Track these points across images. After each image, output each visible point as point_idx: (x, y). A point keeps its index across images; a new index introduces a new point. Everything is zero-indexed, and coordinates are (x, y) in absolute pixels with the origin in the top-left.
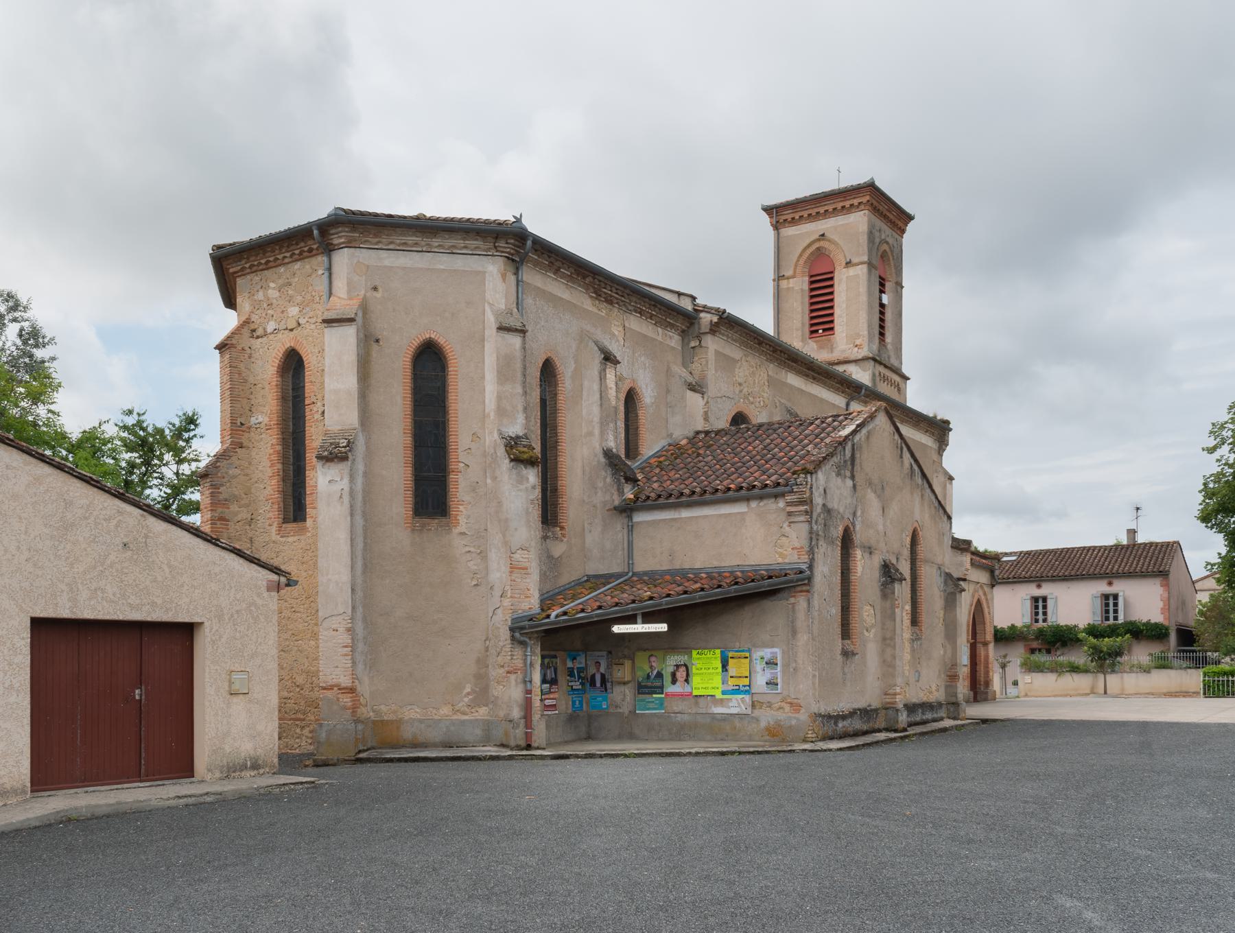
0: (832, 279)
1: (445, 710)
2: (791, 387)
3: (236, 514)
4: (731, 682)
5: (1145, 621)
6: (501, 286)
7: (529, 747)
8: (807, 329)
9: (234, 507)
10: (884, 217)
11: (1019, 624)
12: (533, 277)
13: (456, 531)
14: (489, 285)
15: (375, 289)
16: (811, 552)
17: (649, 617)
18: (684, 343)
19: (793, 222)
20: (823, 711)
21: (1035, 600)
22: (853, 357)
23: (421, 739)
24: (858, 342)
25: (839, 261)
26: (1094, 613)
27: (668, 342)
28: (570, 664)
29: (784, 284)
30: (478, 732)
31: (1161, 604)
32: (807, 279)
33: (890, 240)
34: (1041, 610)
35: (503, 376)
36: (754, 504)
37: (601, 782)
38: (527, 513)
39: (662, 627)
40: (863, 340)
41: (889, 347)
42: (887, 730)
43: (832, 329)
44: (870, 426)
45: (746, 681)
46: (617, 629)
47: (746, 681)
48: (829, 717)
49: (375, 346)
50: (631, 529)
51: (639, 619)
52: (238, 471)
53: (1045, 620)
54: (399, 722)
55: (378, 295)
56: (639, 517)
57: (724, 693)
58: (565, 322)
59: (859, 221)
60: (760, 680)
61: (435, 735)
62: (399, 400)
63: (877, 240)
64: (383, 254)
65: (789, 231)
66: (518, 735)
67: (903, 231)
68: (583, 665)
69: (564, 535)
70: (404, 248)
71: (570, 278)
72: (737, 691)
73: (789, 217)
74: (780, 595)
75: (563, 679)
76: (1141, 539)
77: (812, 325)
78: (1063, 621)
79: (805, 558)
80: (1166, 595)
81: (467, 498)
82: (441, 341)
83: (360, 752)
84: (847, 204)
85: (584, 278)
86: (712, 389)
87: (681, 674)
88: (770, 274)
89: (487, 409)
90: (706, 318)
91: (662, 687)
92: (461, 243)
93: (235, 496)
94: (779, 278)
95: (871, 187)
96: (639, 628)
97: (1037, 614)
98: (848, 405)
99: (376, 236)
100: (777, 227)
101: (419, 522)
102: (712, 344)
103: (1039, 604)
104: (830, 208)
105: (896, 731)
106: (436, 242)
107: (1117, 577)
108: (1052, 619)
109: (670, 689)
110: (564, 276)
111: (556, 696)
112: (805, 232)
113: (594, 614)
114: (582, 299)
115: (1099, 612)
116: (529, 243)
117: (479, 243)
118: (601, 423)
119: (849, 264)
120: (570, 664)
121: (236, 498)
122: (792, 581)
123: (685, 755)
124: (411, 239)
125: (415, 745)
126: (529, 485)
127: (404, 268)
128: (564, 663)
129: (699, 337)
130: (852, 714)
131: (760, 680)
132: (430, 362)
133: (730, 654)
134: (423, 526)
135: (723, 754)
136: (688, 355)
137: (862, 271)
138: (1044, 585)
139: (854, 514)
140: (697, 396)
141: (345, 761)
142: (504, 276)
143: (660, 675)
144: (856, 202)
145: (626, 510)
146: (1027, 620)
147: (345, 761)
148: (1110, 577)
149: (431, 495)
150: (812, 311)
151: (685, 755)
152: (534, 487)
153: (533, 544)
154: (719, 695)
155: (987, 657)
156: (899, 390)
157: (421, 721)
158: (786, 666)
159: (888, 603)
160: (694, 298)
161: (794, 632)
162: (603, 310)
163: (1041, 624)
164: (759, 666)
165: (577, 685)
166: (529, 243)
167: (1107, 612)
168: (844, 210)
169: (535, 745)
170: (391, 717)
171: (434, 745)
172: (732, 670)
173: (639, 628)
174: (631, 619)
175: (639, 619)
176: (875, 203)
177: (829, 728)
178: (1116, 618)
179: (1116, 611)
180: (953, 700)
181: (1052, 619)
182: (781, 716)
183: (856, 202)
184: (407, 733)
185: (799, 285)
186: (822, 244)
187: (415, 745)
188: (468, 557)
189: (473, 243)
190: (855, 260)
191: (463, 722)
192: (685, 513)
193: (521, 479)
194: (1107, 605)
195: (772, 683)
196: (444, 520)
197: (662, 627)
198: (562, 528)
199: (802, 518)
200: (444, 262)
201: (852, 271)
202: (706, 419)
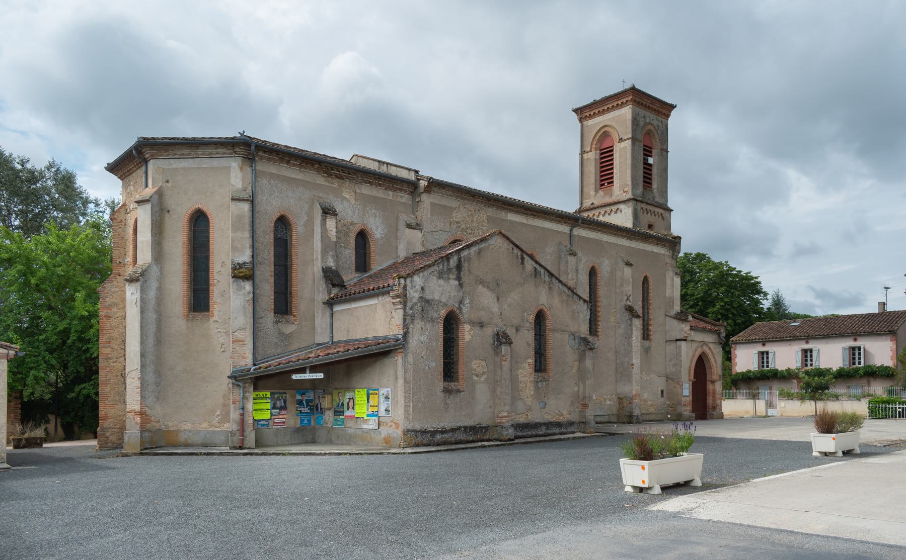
0: (612, 150)
1: (205, 425)
2: (511, 222)
3: (116, 313)
4: (371, 409)
5: (879, 365)
6: (240, 175)
7: (241, 448)
8: (598, 183)
9: (115, 310)
10: (646, 107)
11: (793, 367)
12: (263, 166)
13: (212, 320)
14: (233, 175)
15: (167, 182)
16: (406, 326)
17: (314, 369)
18: (413, 200)
19: (590, 117)
20: (418, 427)
21: (805, 351)
22: (622, 199)
23: (190, 442)
24: (626, 189)
25: (616, 139)
26: (844, 360)
27: (399, 199)
28: (299, 397)
29: (585, 156)
30: (223, 438)
31: (891, 354)
32: (598, 152)
33: (655, 123)
34: (809, 358)
35: (236, 228)
36: (380, 298)
37: (297, 469)
38: (244, 308)
39: (320, 376)
40: (629, 188)
41: (655, 191)
42: (496, 440)
43: (612, 182)
44: (483, 245)
45: (376, 409)
46: (295, 377)
47: (376, 409)
48: (425, 432)
49: (167, 215)
50: (332, 315)
51: (308, 371)
52: (117, 289)
53: (811, 365)
54: (178, 431)
55: (169, 185)
56: (337, 308)
57: (368, 416)
58: (287, 195)
59: (626, 112)
60: (382, 408)
61: (197, 439)
62: (180, 244)
63: (642, 124)
64: (172, 161)
65: (590, 123)
66: (236, 439)
67: (668, 116)
68: (312, 397)
69: (296, 320)
70: (182, 157)
71: (301, 166)
72: (372, 415)
73: (588, 114)
74: (392, 355)
75: (292, 407)
76: (890, 308)
77: (602, 181)
78: (823, 366)
79: (401, 332)
80: (895, 347)
81: (219, 300)
82: (205, 209)
83: (146, 449)
84: (620, 103)
85: (313, 165)
86: (426, 227)
87: (351, 404)
88: (579, 152)
89: (228, 247)
90: (423, 183)
91: (343, 412)
92: (214, 151)
93: (115, 303)
94: (583, 152)
95: (634, 90)
96: (308, 376)
97: (806, 361)
98: (571, 230)
99: (166, 151)
100: (581, 120)
101: (192, 315)
102: (427, 200)
103: (763, 355)
104: (610, 106)
105: (501, 441)
106: (200, 152)
107: (859, 335)
108: (816, 364)
109: (347, 413)
110: (294, 165)
111: (285, 416)
112: (596, 123)
113: (283, 368)
114: (320, 180)
115: (847, 359)
116: (253, 148)
117: (224, 150)
118: (322, 252)
119: (621, 140)
120: (299, 397)
121: (116, 305)
122: (390, 346)
123: (318, 455)
124: (186, 151)
125: (186, 445)
126: (246, 292)
127: (184, 169)
128: (294, 397)
129: (419, 195)
130: (453, 430)
131: (382, 408)
132: (199, 222)
133: (371, 392)
134: (194, 317)
135: (340, 454)
136: (415, 206)
137: (628, 144)
138: (811, 341)
139: (461, 302)
140: (417, 232)
141: (135, 454)
142: (241, 169)
143: (343, 405)
144: (624, 100)
145: (330, 303)
146: (799, 365)
147: (135, 454)
148: (855, 335)
149: (199, 300)
150: (602, 172)
151: (318, 455)
152: (249, 293)
153: (248, 326)
154: (366, 418)
155: (714, 390)
156: (663, 218)
157: (190, 431)
158: (393, 399)
159: (498, 359)
160: (417, 172)
161: (397, 378)
162: (336, 183)
163: (809, 368)
164: (382, 399)
165: (305, 410)
166: (253, 148)
167: (854, 359)
168: (618, 106)
169: (246, 446)
170: (175, 428)
171: (197, 446)
172: (371, 403)
173: (308, 376)
174: (302, 370)
175: (308, 371)
176: (638, 100)
177: (427, 439)
178: (859, 363)
179: (860, 359)
180: (584, 420)
181: (816, 364)
182: (391, 431)
183: (624, 100)
184: (182, 438)
185: (592, 156)
186: (606, 129)
187: (186, 445)
188: (219, 335)
189: (220, 150)
190: (624, 138)
191: (214, 432)
192: (354, 305)
193: (240, 288)
194: (854, 354)
195: (387, 410)
196: (206, 313)
197: (320, 376)
198: (295, 316)
199: (399, 306)
200: (206, 163)
201: (623, 144)
202: (423, 246)
